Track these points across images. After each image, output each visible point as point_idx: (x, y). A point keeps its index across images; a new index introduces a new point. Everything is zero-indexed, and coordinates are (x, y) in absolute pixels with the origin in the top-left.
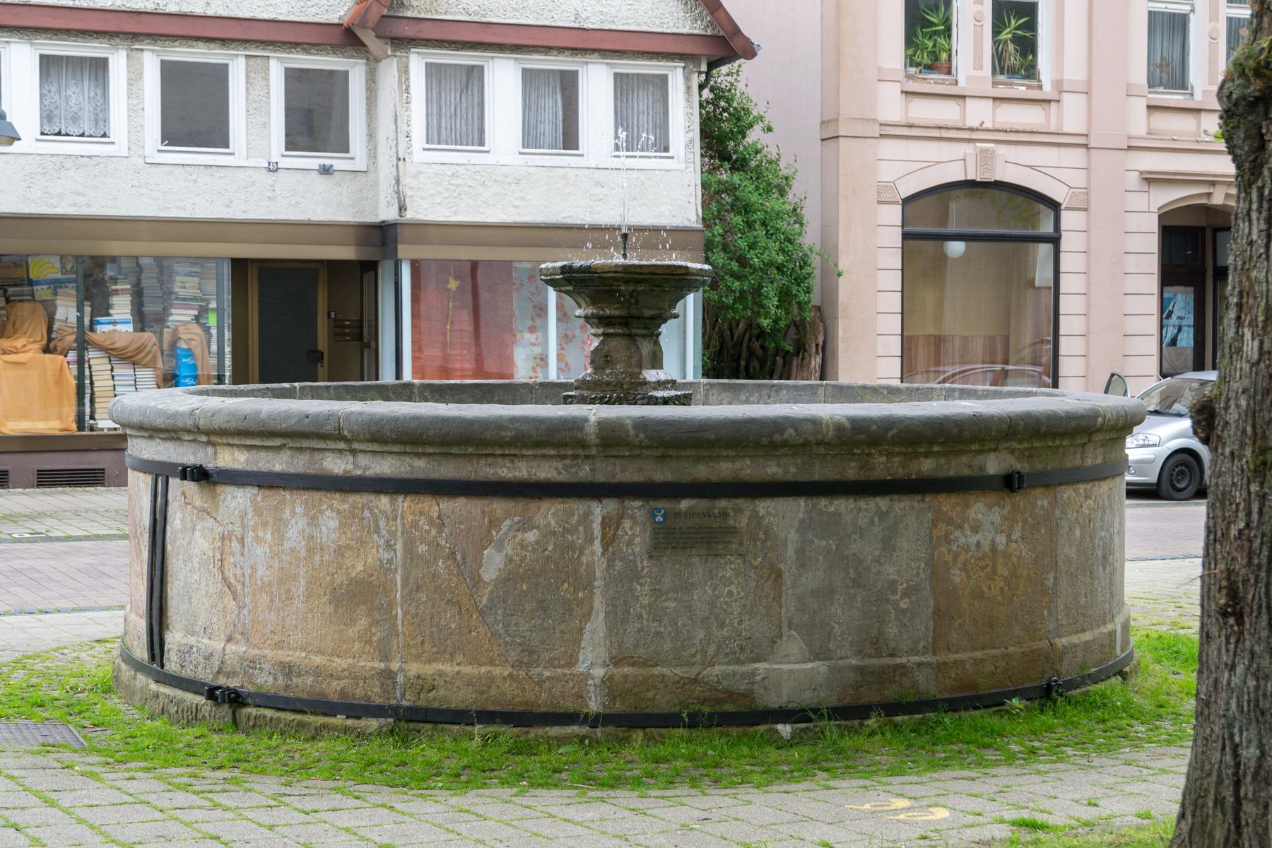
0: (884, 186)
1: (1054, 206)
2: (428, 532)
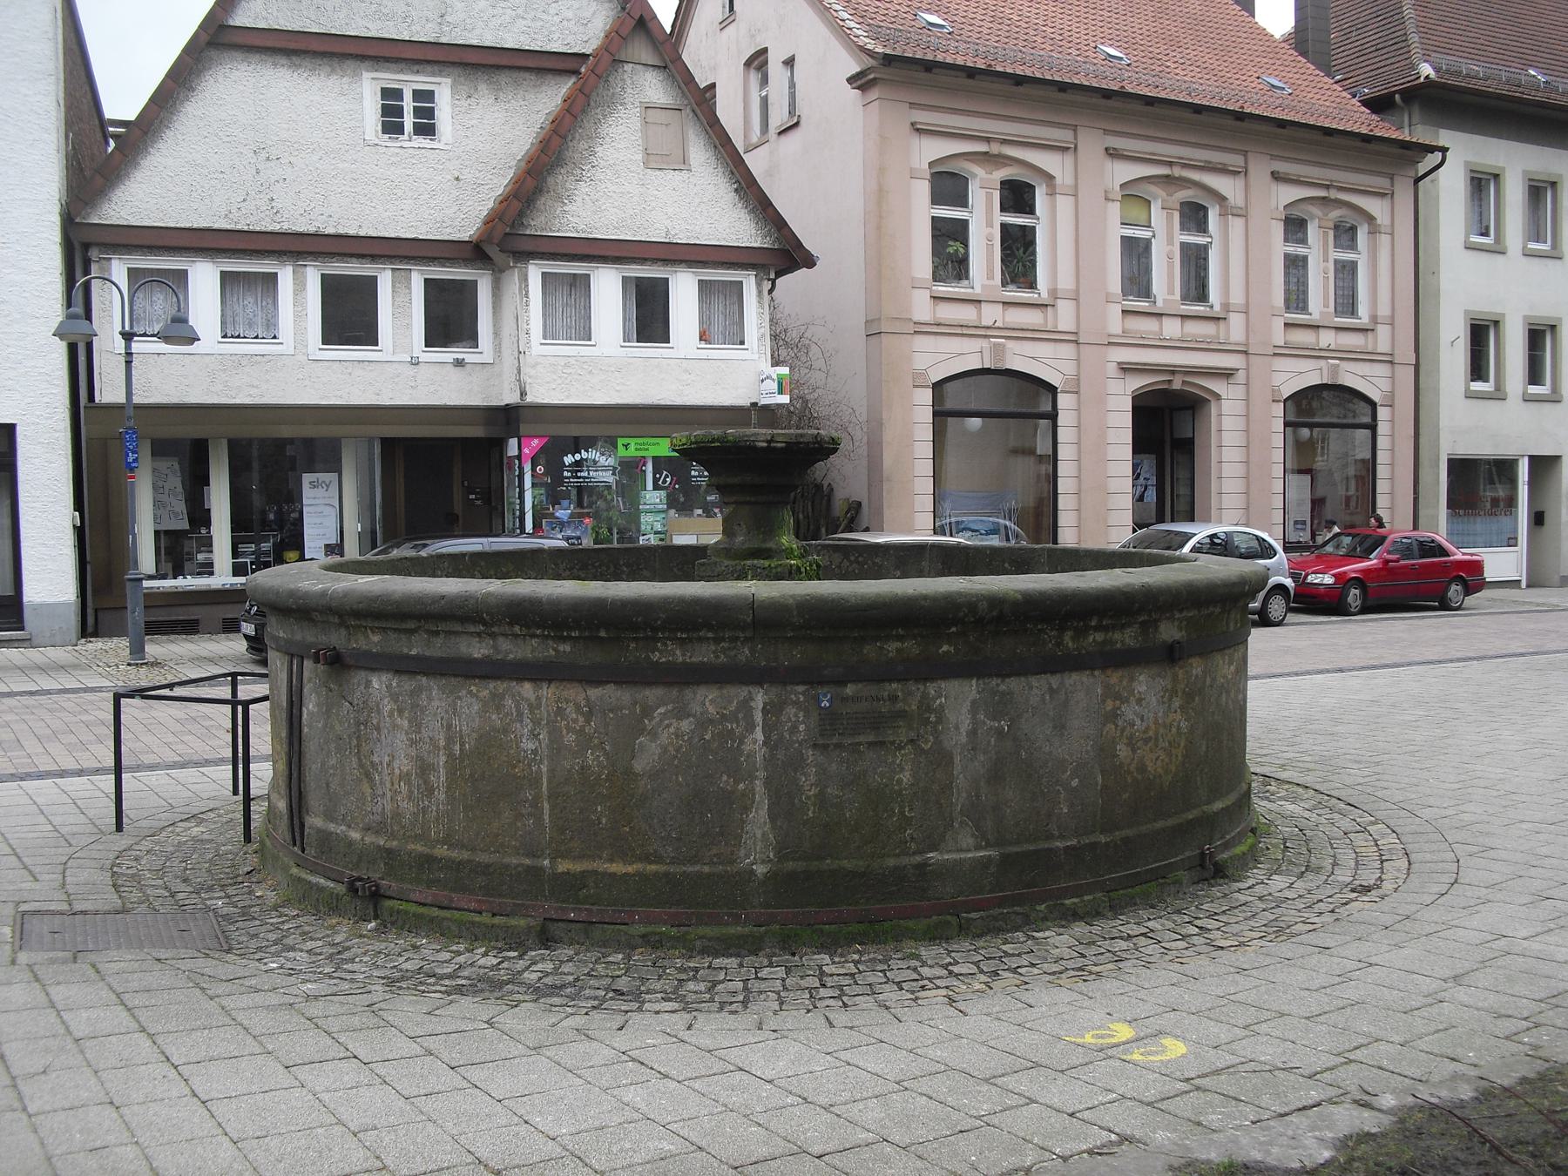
0: (923, 374)
1: (1052, 390)
2: (575, 721)
